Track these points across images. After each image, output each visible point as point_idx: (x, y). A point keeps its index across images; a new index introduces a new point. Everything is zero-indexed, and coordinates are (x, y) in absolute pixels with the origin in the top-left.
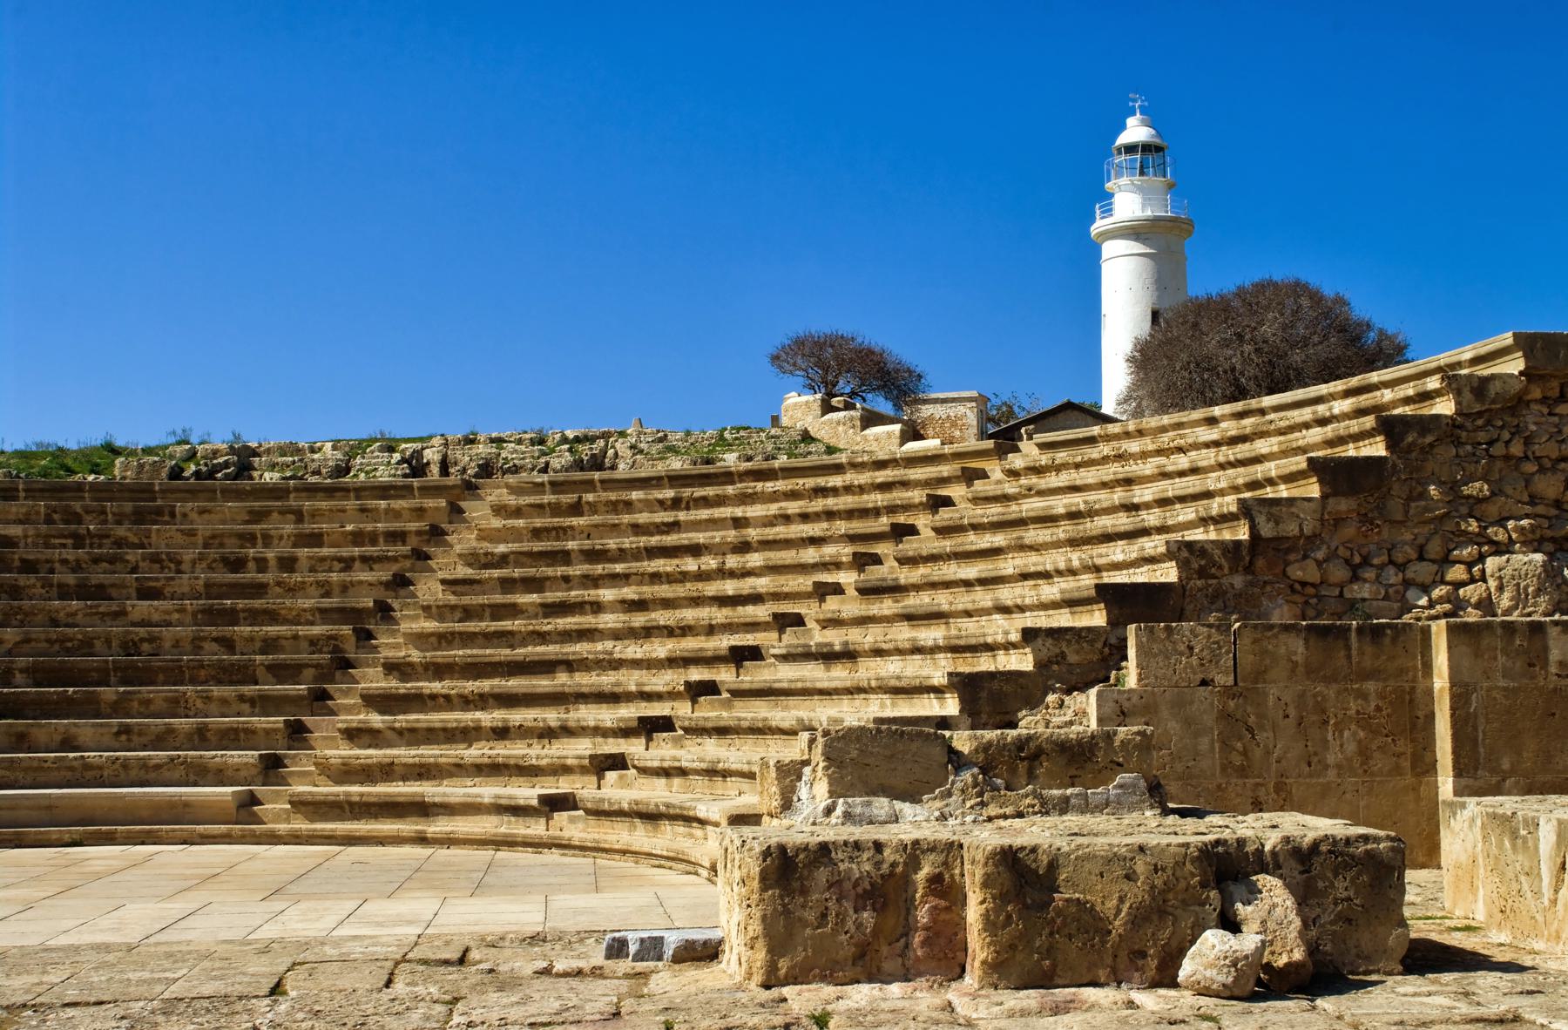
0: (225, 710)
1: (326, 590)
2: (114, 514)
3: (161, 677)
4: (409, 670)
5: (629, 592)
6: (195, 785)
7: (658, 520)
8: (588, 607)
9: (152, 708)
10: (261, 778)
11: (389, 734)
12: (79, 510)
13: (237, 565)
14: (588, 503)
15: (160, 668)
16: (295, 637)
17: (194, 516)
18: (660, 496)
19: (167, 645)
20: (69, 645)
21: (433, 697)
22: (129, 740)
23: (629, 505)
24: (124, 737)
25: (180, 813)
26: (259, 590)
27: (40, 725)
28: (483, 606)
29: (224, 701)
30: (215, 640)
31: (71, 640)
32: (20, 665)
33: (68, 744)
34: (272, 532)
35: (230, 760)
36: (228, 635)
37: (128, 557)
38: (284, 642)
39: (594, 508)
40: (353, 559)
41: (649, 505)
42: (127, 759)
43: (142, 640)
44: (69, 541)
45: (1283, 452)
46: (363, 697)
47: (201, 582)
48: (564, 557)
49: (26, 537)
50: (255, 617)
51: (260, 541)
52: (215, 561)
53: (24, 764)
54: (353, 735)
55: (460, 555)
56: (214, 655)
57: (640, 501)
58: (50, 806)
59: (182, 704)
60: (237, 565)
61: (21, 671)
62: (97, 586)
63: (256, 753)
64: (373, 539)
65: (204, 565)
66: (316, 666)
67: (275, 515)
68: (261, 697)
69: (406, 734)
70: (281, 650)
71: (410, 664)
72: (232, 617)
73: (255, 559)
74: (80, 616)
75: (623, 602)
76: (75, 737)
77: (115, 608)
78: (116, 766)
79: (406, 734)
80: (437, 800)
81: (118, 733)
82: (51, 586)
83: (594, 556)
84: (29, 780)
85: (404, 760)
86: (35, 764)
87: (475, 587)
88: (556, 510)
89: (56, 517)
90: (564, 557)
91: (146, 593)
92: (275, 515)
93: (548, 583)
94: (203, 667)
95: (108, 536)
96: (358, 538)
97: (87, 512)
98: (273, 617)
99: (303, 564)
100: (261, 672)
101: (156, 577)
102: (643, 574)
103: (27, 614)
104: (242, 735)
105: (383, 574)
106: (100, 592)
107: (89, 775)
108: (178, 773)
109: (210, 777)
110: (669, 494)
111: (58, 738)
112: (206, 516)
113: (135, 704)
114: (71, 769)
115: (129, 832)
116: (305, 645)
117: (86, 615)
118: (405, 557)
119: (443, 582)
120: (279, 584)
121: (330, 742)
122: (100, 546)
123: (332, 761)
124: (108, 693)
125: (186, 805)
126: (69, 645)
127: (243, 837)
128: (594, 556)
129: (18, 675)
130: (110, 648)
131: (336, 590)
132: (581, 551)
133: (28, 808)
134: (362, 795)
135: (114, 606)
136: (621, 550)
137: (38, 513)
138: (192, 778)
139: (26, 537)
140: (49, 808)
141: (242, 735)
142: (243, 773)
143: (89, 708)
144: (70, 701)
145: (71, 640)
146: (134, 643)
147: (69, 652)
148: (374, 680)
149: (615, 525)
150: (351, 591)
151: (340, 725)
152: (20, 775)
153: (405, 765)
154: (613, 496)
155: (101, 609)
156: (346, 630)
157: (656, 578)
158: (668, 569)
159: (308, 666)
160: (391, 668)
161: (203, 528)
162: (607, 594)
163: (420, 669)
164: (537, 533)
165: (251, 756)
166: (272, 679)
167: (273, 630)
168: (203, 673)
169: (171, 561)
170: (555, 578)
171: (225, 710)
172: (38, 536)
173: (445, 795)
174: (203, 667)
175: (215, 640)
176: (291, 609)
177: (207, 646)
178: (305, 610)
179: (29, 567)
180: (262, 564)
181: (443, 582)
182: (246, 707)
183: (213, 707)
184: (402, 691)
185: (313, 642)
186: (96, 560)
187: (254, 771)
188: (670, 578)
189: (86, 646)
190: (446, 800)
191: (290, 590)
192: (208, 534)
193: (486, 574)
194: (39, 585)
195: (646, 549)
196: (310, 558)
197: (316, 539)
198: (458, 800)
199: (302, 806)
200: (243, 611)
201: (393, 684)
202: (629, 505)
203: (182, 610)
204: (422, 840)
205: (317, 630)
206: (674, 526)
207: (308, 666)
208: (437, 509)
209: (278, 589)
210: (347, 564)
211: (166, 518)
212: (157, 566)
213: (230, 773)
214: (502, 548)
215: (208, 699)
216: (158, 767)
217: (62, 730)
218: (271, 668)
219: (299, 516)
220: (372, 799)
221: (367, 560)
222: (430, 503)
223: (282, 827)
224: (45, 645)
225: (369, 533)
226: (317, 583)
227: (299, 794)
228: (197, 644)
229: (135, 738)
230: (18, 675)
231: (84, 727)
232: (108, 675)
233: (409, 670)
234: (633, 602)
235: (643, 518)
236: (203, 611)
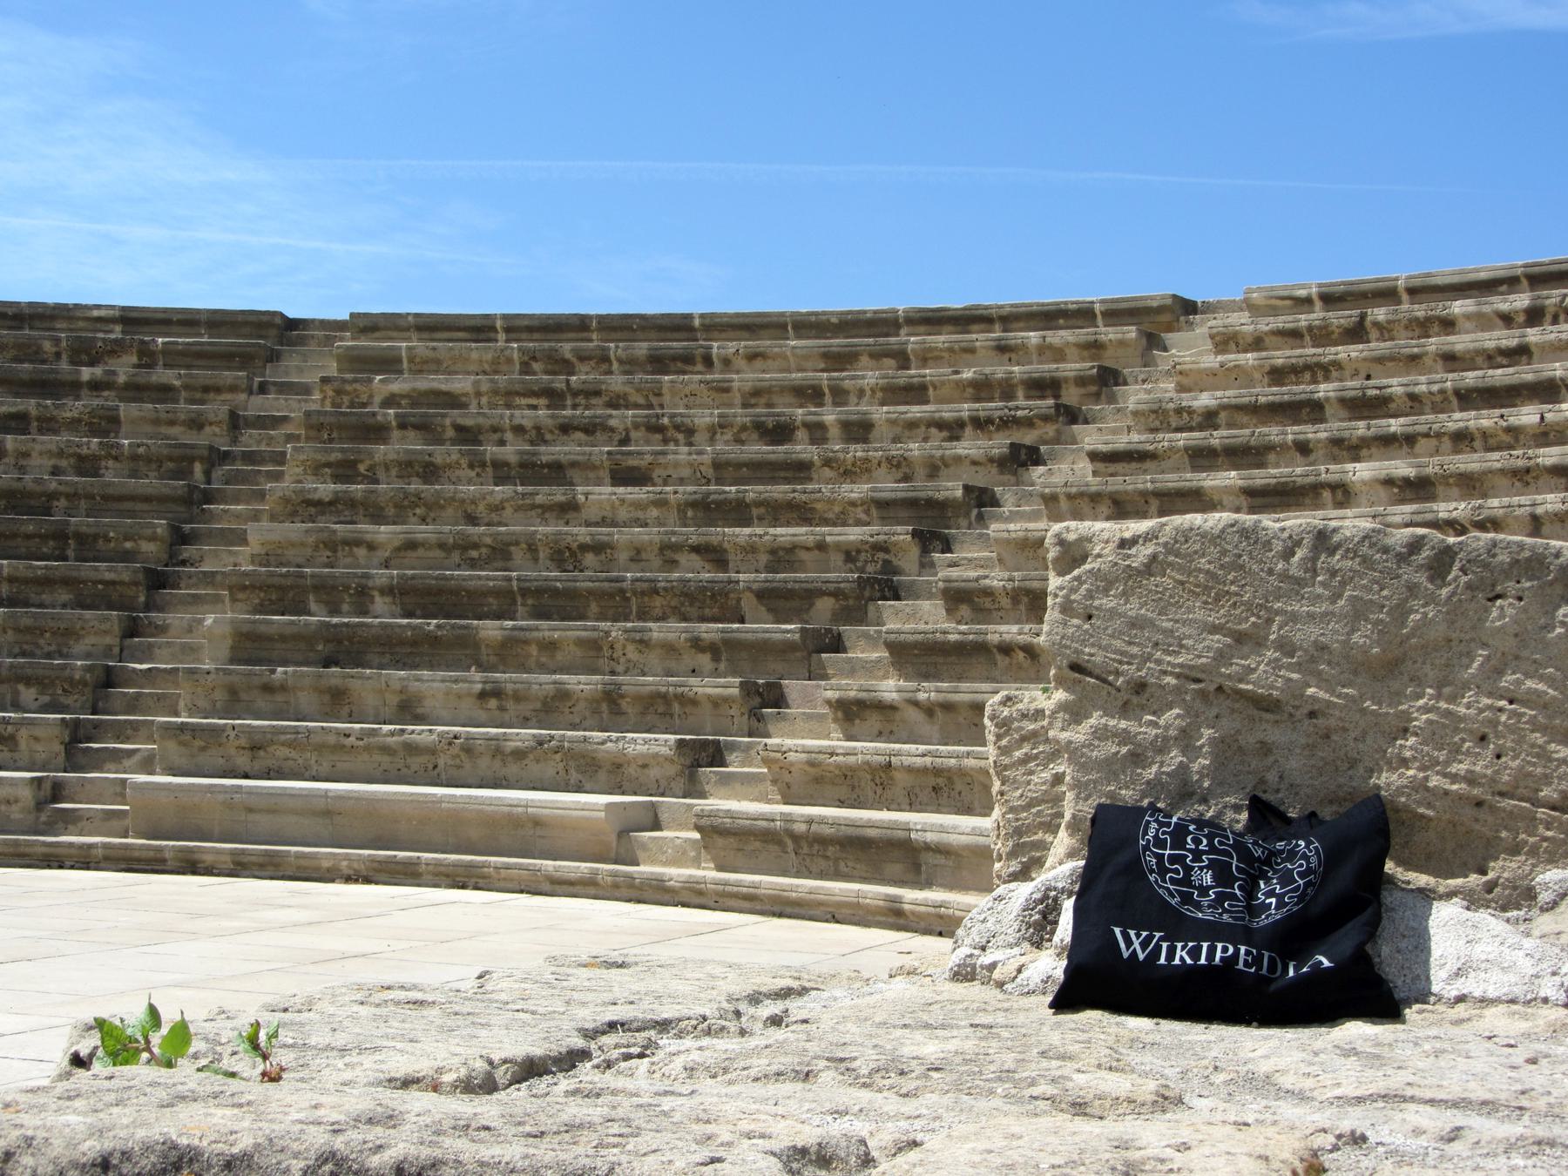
0: (673, 665)
1: (899, 466)
2: (620, 361)
3: (594, 608)
4: (987, 603)
5: (1402, 467)
6: (579, 789)
7: (1490, 345)
8: (1327, 494)
9: (559, 656)
10: (679, 785)
11: (914, 715)
12: (568, 356)
13: (780, 433)
14: (1376, 324)
15: (590, 592)
16: (821, 546)
17: (740, 363)
18: (1504, 307)
19: (623, 556)
20: (474, 554)
21: (1006, 649)
22: (502, 709)
23: (1448, 325)
24: (493, 703)
25: (527, 835)
26: (799, 470)
27: (362, 677)
28: (1144, 494)
29: (670, 649)
30: (696, 549)
31: (476, 546)
32: (379, 582)
33: (409, 710)
34: (847, 384)
35: (630, 749)
36: (715, 540)
37: (612, 423)
38: (803, 555)
39: (1385, 331)
40: (960, 424)
41: (1482, 321)
42: (469, 738)
43: (584, 548)
44: (543, 401)
45: (1405, 1101)
46: (890, 646)
47: (707, 459)
48: (1313, 410)
49: (478, 394)
50: (778, 512)
51: (828, 398)
52: (744, 428)
53: (315, 739)
54: (851, 713)
55: (1135, 413)
56: (694, 572)
57: (1468, 317)
58: (328, 811)
59: (606, 652)
60: (780, 433)
61: (382, 592)
62: (550, 466)
63: (672, 737)
64: (1007, 390)
65: (729, 436)
66: (836, 594)
67: (864, 360)
68: (726, 642)
69: (939, 713)
70: (791, 566)
71: (988, 593)
72: (739, 513)
73: (806, 425)
74: (508, 511)
75: (1389, 482)
76: (420, 699)
77: (560, 498)
78: (455, 750)
79: (939, 713)
80: (930, 837)
81: (483, 695)
82: (483, 465)
83: (1366, 406)
84: (325, 767)
85: (907, 761)
86: (332, 739)
87: (1148, 464)
88: (1321, 336)
89: (536, 366)
90: (1313, 410)
91: (623, 476)
92: (864, 360)
93: (1272, 457)
94: (656, 592)
95: (597, 393)
96: (981, 388)
97: (582, 359)
98: (802, 513)
99: (882, 431)
100: (748, 603)
101: (643, 450)
102: (1439, 435)
103: (429, 507)
104: (676, 707)
105: (998, 444)
106: (557, 472)
107: (417, 762)
108: (550, 769)
109: (602, 776)
110: (1521, 301)
111: (393, 700)
112: (758, 363)
113: (534, 650)
114: (386, 750)
115: (438, 863)
116: (837, 559)
117: (518, 509)
118: (1046, 418)
119: (1094, 456)
120: (828, 463)
121: (814, 724)
122: (587, 407)
123: (792, 756)
124: (491, 630)
125: (537, 822)
126: (474, 554)
127: (616, 886)
128: (1366, 406)
129: (378, 599)
130: (536, 560)
131: (921, 472)
132: (1343, 401)
133: (295, 812)
134: (810, 821)
135: (558, 494)
136: (1413, 397)
137: (510, 361)
138: (574, 776)
139: (478, 394)
140: (328, 813)
141: (676, 707)
142: (654, 773)
143: (460, 651)
144: (434, 640)
145: (476, 546)
146: (573, 554)
147: (473, 563)
148: (923, 617)
149: (1414, 358)
150: (944, 472)
151: (829, 694)
152: (312, 757)
153: (910, 769)
154: (1420, 311)
155: (539, 499)
156: (901, 534)
157: (1462, 439)
158: (1485, 423)
159: (822, 593)
160: (959, 598)
161: (745, 378)
162: (1361, 471)
163: (1005, 602)
164: (1276, 375)
165: (662, 743)
166: (771, 617)
167: (785, 533)
168: (658, 602)
169: (677, 428)
170: (1283, 446)
171: (673, 665)
172: (496, 392)
173: (942, 829)
174: (656, 592)
175: (696, 549)
176: (831, 502)
177: (684, 558)
178: (853, 504)
179: (467, 435)
180: (817, 432)
181: (1094, 456)
182: (705, 660)
183: (653, 659)
184: (952, 637)
185: (850, 555)
186: (566, 429)
187: (672, 770)
188: (1488, 440)
189: (500, 553)
190: (945, 838)
191: (846, 473)
192: (748, 386)
193: (1166, 440)
194: (464, 462)
195: (1457, 393)
196: (893, 422)
197: (916, 392)
198: (964, 839)
199: (722, 838)
200: (758, 504)
201: (955, 630)
202: (1448, 325)
203: (661, 503)
204: (896, 918)
205: (853, 534)
206: (1521, 353)
207: (822, 593)
208: (1122, 343)
209: (827, 472)
210: (953, 430)
211: (699, 367)
212: (659, 437)
213: (632, 770)
214: (1205, 400)
215: (644, 644)
216: (519, 754)
217: (397, 686)
218: (763, 595)
219: (903, 359)
220: (827, 831)
221: (980, 424)
222: (1108, 333)
223: (677, 874)
224: (438, 553)
225: (1000, 382)
226: (889, 460)
227: (712, 814)
228: (668, 552)
229: (510, 705)
230: (378, 599)
231: (430, 682)
232: (514, 602)
233: (987, 603)
234: (1407, 483)
235: (1461, 342)
236: (694, 505)
